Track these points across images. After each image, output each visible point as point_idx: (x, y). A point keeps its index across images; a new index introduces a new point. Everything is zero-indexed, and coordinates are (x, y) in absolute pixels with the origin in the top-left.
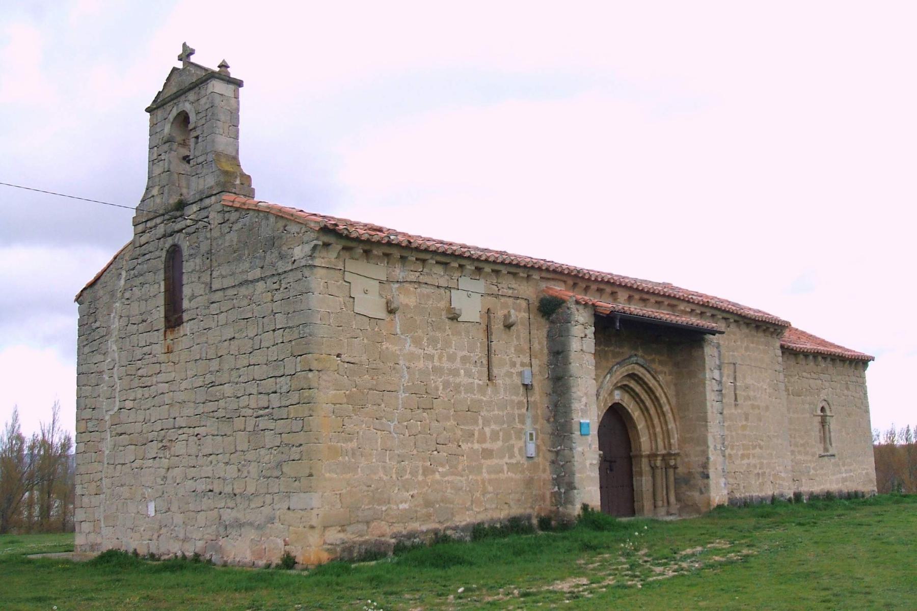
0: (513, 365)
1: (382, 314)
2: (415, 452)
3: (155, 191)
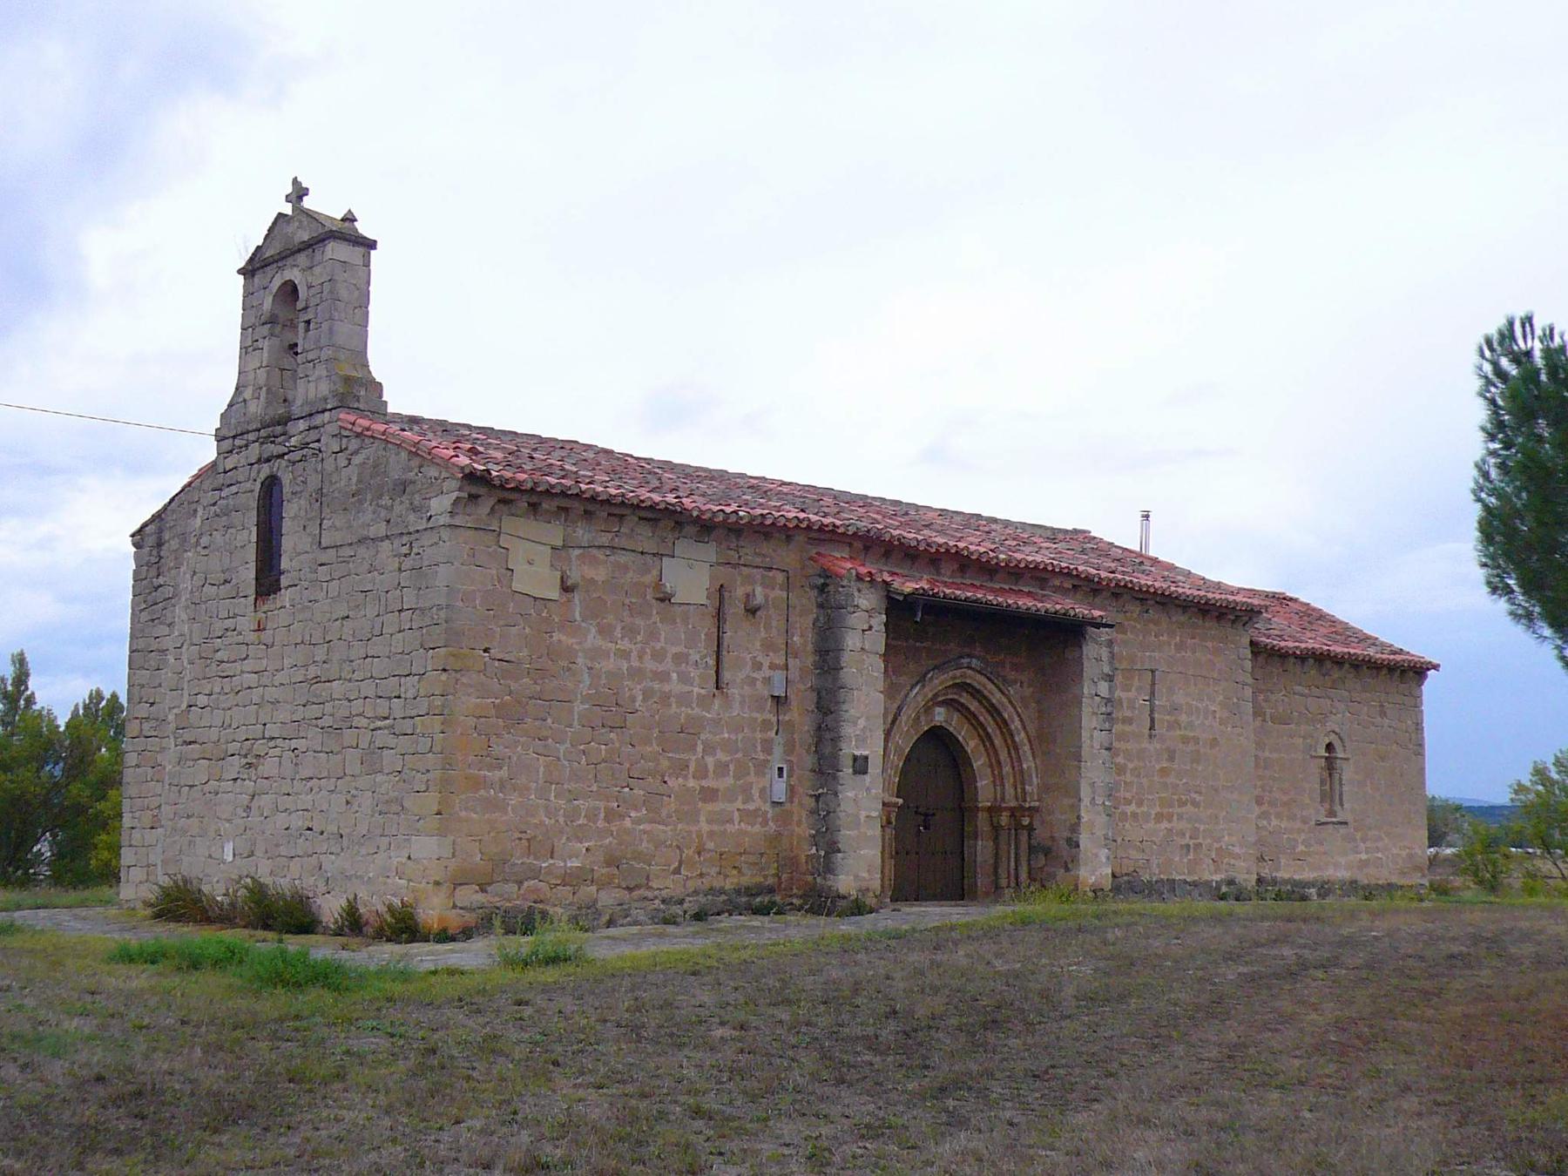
0: (758, 666)
1: (554, 594)
2: (594, 788)
3: (248, 394)
